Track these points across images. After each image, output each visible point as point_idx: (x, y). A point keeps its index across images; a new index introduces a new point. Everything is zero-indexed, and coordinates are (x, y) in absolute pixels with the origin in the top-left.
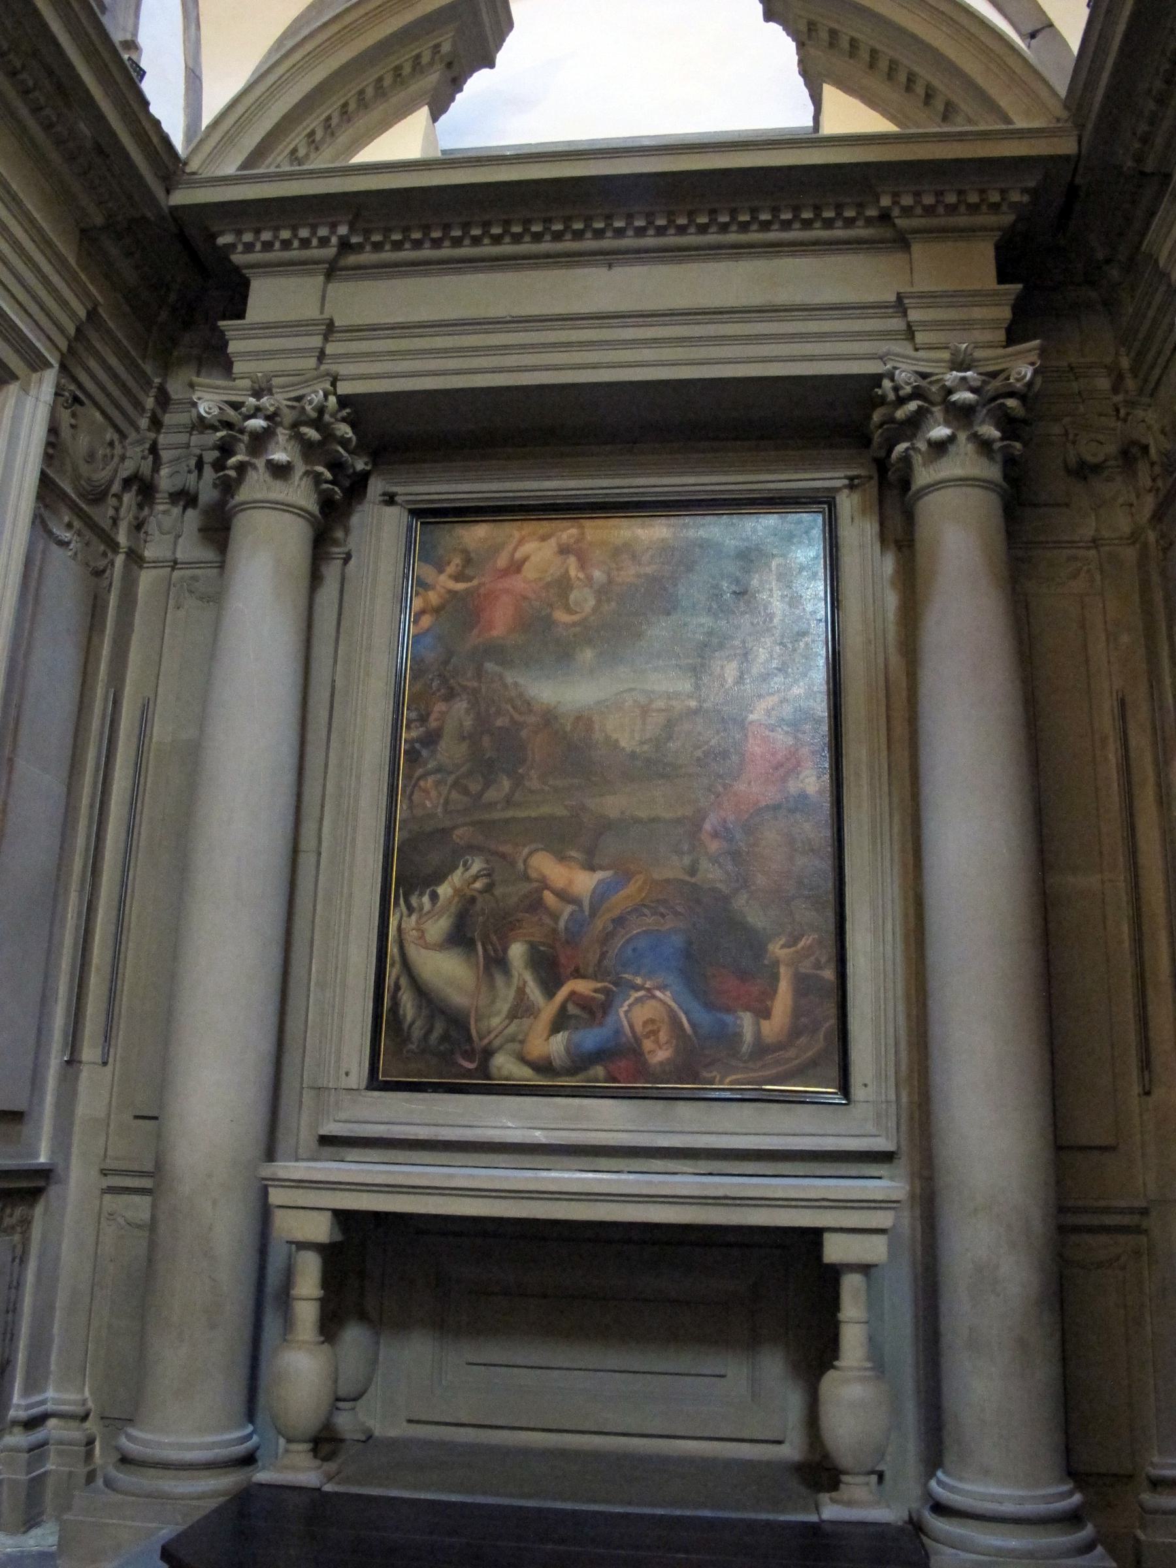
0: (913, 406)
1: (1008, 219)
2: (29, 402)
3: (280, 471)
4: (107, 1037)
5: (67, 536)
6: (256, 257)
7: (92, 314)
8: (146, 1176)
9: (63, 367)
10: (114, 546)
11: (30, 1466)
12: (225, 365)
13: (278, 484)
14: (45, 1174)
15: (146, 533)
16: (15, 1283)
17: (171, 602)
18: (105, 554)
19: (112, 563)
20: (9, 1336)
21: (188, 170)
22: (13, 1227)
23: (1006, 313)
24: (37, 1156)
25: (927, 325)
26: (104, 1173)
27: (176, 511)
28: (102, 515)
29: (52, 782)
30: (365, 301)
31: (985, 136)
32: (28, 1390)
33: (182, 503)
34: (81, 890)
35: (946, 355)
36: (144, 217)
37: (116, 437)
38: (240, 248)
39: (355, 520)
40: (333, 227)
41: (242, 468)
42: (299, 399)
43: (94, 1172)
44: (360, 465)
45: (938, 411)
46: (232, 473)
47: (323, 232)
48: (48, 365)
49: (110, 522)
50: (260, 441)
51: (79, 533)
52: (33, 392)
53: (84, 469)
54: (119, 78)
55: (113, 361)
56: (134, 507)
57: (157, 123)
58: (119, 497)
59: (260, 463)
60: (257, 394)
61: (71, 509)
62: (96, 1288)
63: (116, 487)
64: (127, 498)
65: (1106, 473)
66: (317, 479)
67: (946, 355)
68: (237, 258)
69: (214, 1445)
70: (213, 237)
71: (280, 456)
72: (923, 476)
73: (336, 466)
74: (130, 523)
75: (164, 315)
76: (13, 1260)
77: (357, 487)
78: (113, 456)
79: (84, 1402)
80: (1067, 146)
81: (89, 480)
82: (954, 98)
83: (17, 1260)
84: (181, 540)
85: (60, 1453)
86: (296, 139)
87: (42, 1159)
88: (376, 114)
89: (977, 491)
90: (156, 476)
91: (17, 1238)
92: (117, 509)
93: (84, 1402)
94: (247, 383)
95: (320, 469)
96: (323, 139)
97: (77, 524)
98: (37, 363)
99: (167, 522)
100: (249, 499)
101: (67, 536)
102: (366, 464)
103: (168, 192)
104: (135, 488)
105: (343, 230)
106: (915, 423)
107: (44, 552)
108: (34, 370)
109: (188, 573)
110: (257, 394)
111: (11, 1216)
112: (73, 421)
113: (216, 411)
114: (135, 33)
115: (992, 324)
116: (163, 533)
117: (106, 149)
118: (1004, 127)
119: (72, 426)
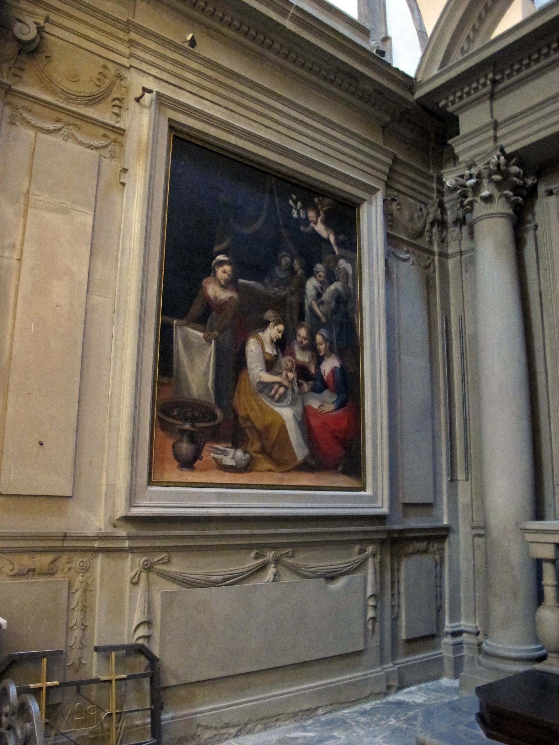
2: (373, 208)
3: (488, 199)
4: (467, 468)
5: (406, 256)
6: (457, 105)
7: (395, 160)
8: (481, 530)
9: (388, 186)
10: (432, 253)
11: (455, 652)
12: (455, 158)
13: (488, 206)
14: (447, 529)
15: (447, 243)
16: (439, 575)
17: (463, 270)
18: (428, 258)
19: (434, 261)
20: (439, 597)
21: (418, 81)
22: (434, 552)
24: (443, 522)
26: (473, 528)
27: (457, 229)
28: (423, 242)
29: (423, 363)
30: (509, 105)
32: (452, 620)
33: (459, 225)
34: (445, 405)
36: (407, 109)
37: (422, 206)
38: (450, 104)
39: (537, 209)
40: (486, 76)
41: (471, 203)
42: (488, 163)
43: (469, 528)
44: (530, 182)
46: (469, 207)
47: (482, 81)
48: (378, 190)
49: (428, 244)
50: (476, 188)
51: (413, 253)
52: (374, 203)
53: (410, 226)
54: (374, 61)
55: (412, 175)
56: (438, 233)
57: (397, 70)
58: (430, 231)
59: (478, 199)
60: (470, 168)
61: (407, 245)
62: (476, 579)
63: (427, 227)
64: (435, 230)
66: (507, 197)
68: (450, 109)
69: (517, 651)
70: (437, 104)
71: (485, 193)
73: (516, 189)
74: (438, 241)
75: (432, 145)
76: (436, 566)
77: (531, 194)
78: (423, 215)
79: (476, 627)
81: (413, 229)
83: (439, 566)
84: (462, 242)
85: (469, 648)
86: (462, 42)
87: (445, 523)
88: (496, 10)
90: (445, 217)
91: (437, 557)
92: (430, 237)
93: (476, 627)
94: (464, 165)
95: (506, 192)
96: (474, 37)
97: (411, 250)
98: (372, 191)
99: (455, 234)
100: (477, 216)
101: (406, 256)
102: (533, 180)
103: (413, 94)
104: (436, 225)
105: (490, 76)
107: (397, 266)
108: (373, 194)
109: (468, 255)
110: (470, 168)
111: (433, 547)
112: (399, 207)
113: (454, 182)
114: (386, 32)
116: (454, 241)
117: (380, 90)
119: (399, 209)
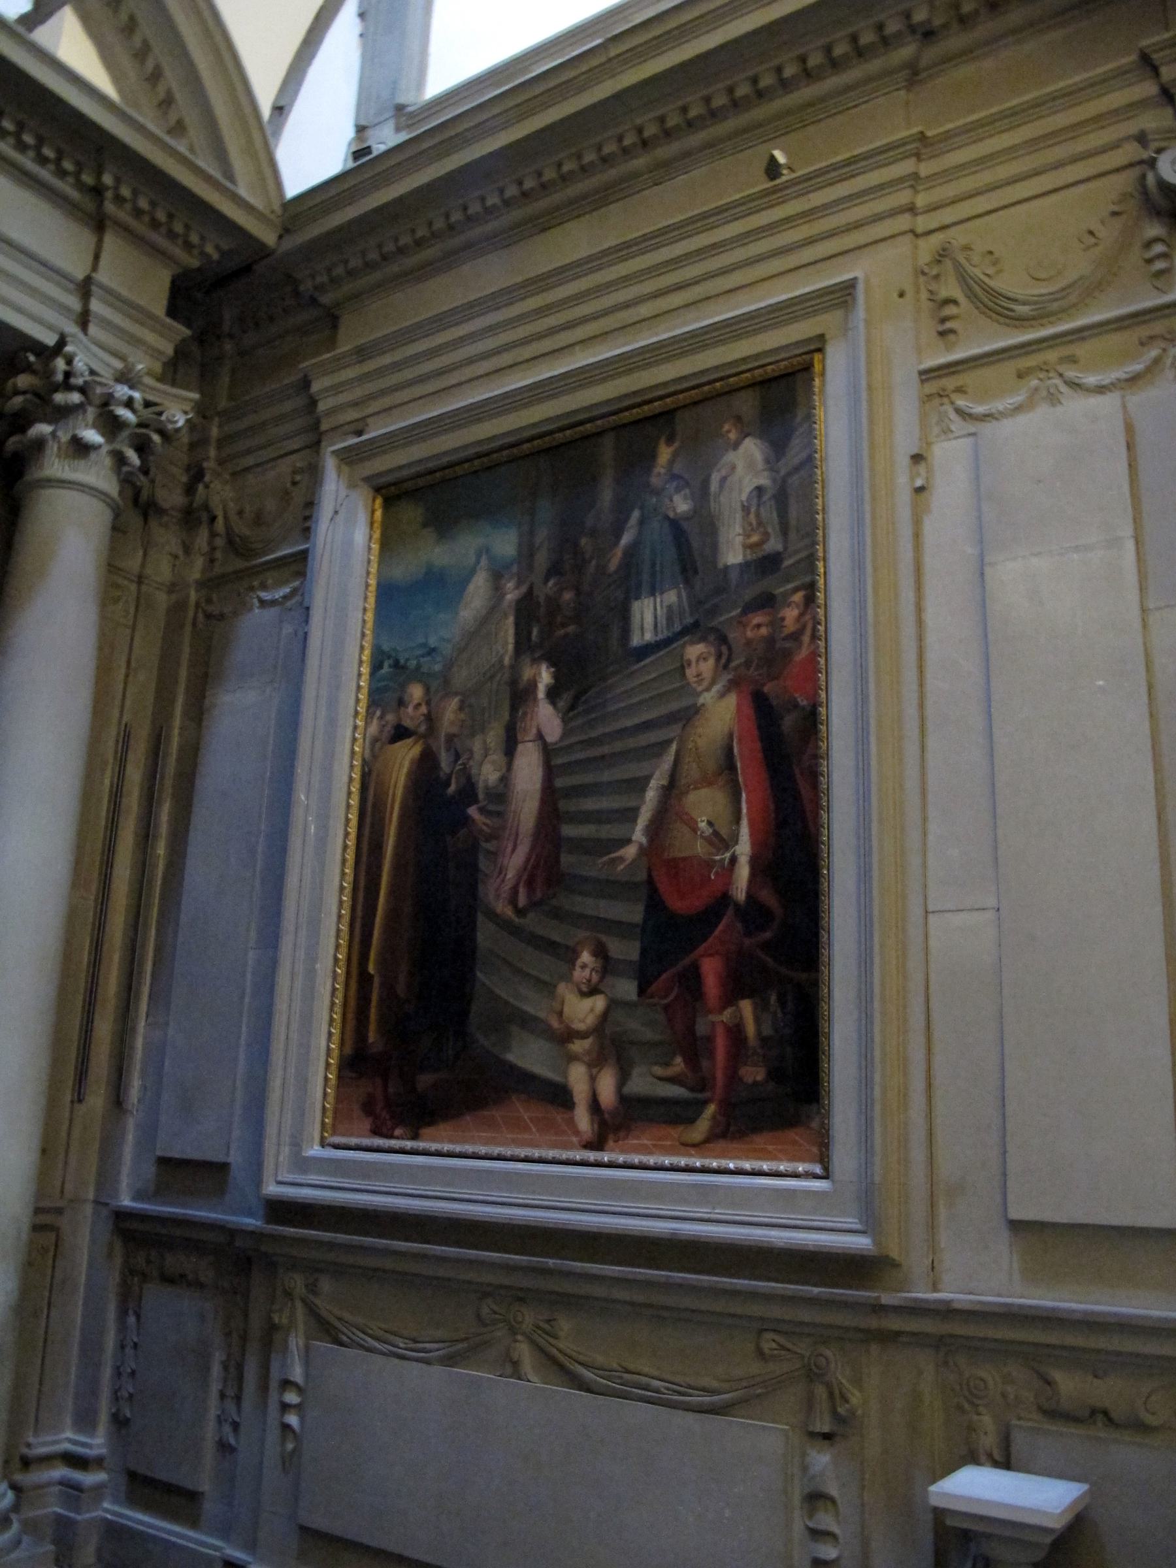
0: (76, 397)
1: (195, 263)
23: (169, 349)
25: (107, 324)
31: (208, 178)
35: (119, 365)
45: (91, 413)
65: (165, 519)
67: (119, 365)
72: (54, 466)
80: (269, 237)
82: (187, 121)
89: (94, 501)
106: (63, 413)
115: (154, 352)
118: (187, 153)
